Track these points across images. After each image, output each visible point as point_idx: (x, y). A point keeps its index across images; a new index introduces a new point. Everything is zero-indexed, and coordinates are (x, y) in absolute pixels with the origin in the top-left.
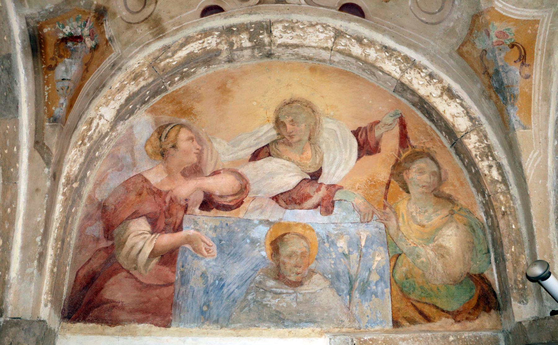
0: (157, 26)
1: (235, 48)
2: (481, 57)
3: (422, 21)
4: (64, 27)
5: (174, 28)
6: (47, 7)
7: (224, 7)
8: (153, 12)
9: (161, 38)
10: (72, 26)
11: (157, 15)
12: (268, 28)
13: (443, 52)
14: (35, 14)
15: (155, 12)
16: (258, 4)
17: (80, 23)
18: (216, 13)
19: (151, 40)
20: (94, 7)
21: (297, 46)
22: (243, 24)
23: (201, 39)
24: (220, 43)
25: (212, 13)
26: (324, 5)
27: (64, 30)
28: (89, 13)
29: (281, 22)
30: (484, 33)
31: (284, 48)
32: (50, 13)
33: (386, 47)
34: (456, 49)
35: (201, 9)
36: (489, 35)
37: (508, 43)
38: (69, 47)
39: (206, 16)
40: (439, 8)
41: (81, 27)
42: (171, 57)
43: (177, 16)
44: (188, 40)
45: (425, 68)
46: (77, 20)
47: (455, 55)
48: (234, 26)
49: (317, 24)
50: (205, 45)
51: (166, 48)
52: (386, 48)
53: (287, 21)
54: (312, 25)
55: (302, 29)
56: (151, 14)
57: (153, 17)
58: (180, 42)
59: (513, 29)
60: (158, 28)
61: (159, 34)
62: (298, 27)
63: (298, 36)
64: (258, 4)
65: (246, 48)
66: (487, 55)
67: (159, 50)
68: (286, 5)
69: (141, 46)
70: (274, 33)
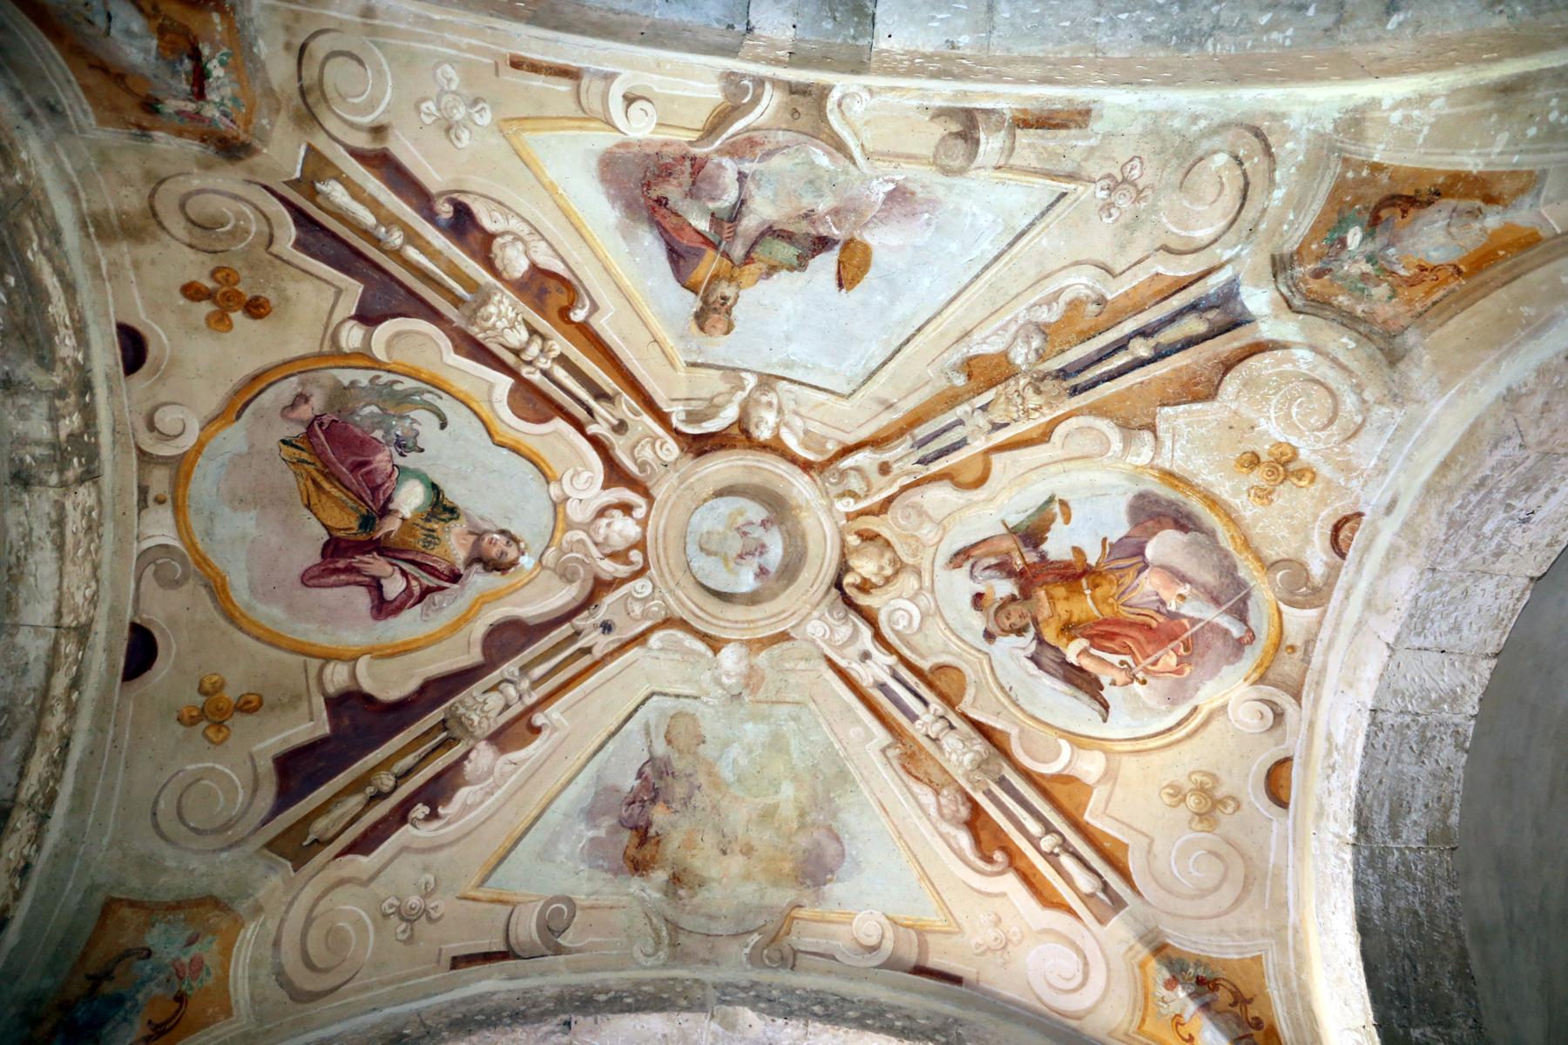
0: (122, 228)
1: (58, 403)
2: (128, 953)
3: (156, 803)
4: (222, 64)
5: (104, 264)
6: (260, 42)
7: (136, 377)
8: (169, 233)
9: (84, 226)
10: (223, 85)
11: (155, 238)
12: (90, 475)
13: (92, 870)
14: (249, 10)
15: (166, 238)
16: (139, 449)
17: (229, 104)
18: (124, 358)
19: (84, 205)
20: (256, 143)
21: (60, 547)
22: (95, 417)
23: (72, 319)
24: (66, 368)
25: (124, 349)
26: (143, 588)
27: (215, 62)
28: (246, 131)
29: (99, 501)
30: (189, 933)
31: (54, 516)
32: (251, 46)
33: (67, 745)
34: (116, 895)
35: (141, 329)
36: (190, 942)
37: (184, 987)
38: (181, 62)
39: (119, 336)
40: (201, 827)
41: (222, 104)
42: (40, 245)
43: (137, 276)
44: (69, 288)
45: (38, 850)
46: (235, 99)
47: (99, 899)
48: (93, 396)
49: (97, 581)
50: (62, 331)
51: (56, 234)
52: (65, 747)
53: (100, 514)
54: (96, 568)
55: (88, 551)
56: (164, 228)
57: (153, 227)
58: (67, 270)
59: (210, 982)
60: (117, 229)
61: (98, 226)
62: (92, 541)
63: (77, 545)
64: (139, 449)
65: (55, 430)
66: (141, 963)
67: (53, 217)
68: (136, 510)
69: (75, 180)
70: (82, 490)
